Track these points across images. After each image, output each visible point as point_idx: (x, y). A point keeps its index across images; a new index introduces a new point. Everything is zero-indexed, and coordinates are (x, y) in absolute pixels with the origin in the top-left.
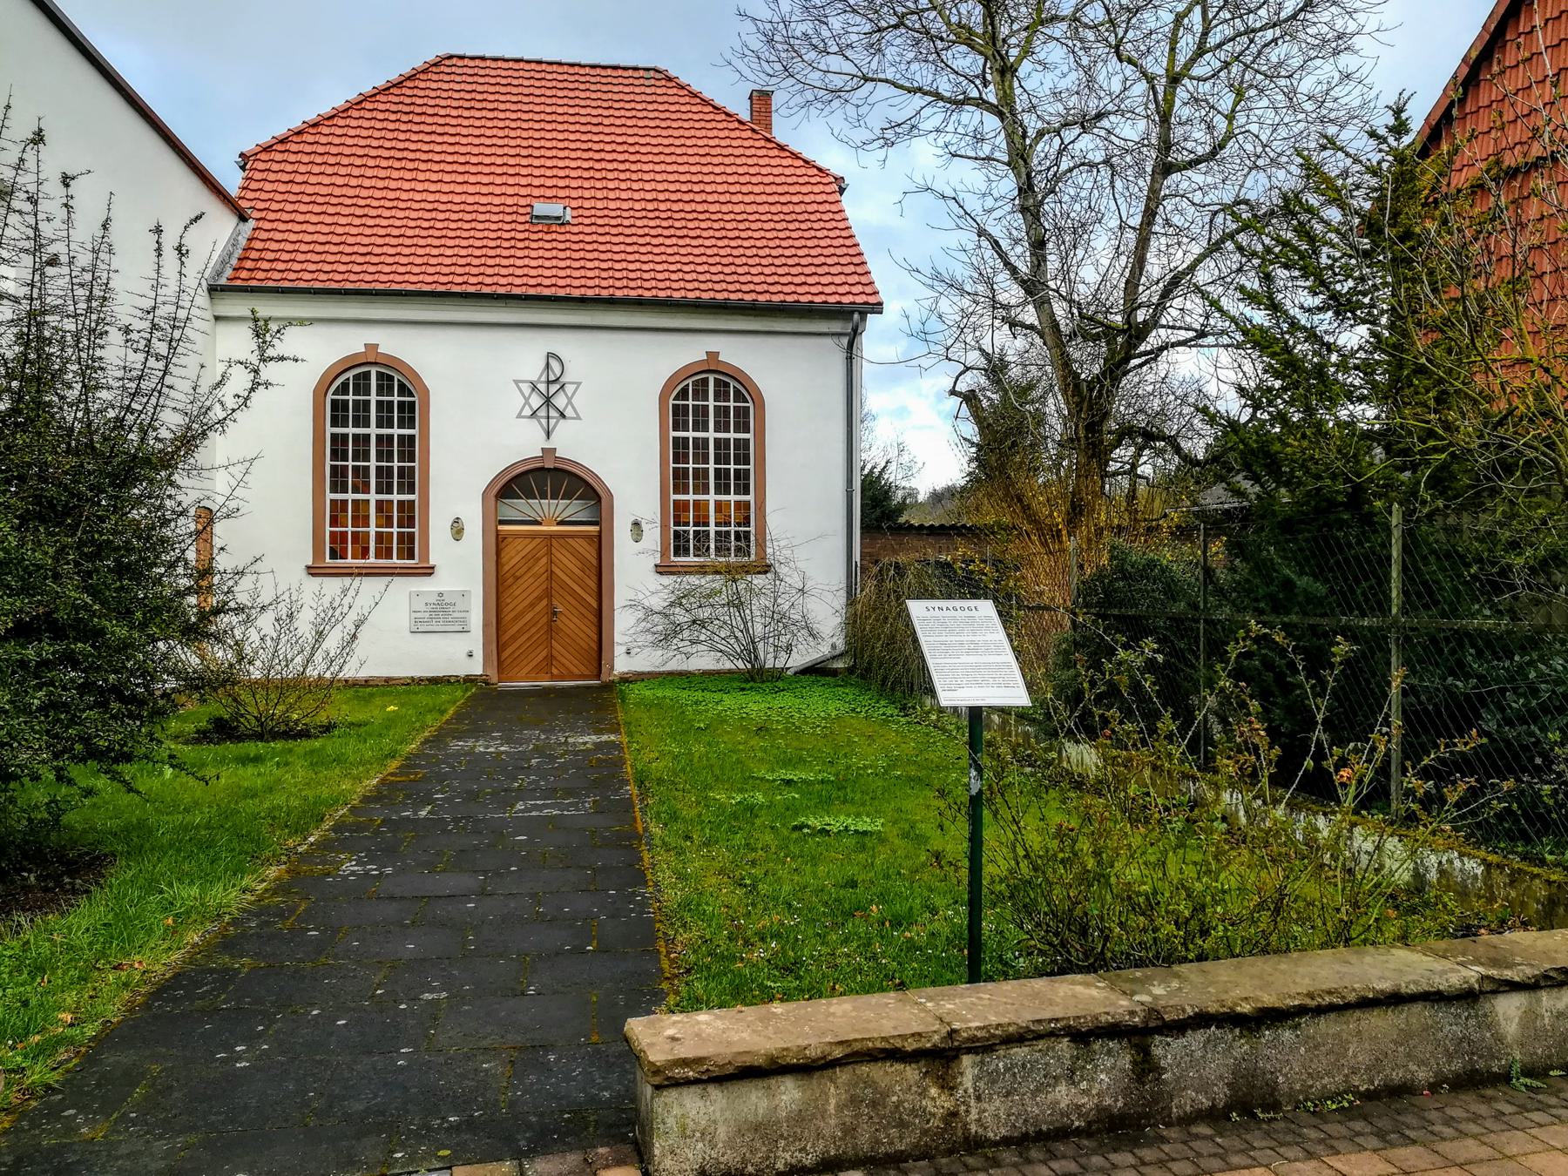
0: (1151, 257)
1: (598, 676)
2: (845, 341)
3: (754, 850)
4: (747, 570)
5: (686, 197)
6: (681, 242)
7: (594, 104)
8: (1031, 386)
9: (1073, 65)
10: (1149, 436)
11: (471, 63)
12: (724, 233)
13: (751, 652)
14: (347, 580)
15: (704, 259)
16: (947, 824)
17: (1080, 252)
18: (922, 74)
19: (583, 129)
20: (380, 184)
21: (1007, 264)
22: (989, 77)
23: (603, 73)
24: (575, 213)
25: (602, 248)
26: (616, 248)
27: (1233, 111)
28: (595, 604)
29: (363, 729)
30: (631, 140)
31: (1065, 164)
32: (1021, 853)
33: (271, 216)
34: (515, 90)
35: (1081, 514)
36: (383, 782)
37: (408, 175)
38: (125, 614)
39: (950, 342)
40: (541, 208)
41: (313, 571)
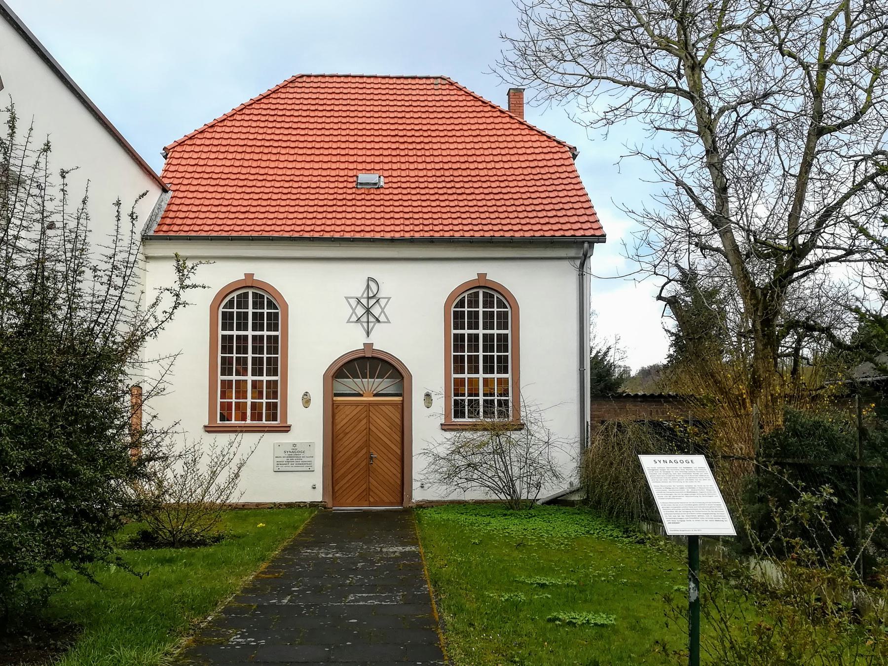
0: (808, 196)
1: (401, 503)
2: (578, 262)
3: (520, 636)
4: (506, 427)
5: (464, 166)
6: (460, 198)
7: (399, 103)
8: (716, 291)
9: (746, 60)
10: (810, 329)
11: (316, 80)
12: (490, 190)
13: (510, 485)
14: (233, 435)
15: (476, 209)
16: (670, 622)
17: (755, 196)
18: (634, 73)
19: (392, 121)
20: (255, 164)
21: (699, 205)
22: (682, 72)
23: (406, 82)
24: (387, 180)
25: (406, 204)
26: (415, 204)
27: (871, 86)
28: (399, 452)
29: (241, 541)
30: (425, 128)
31: (740, 132)
32: (727, 644)
33: (183, 188)
34: (345, 97)
35: (760, 387)
36: (257, 577)
37: (274, 158)
38: (91, 460)
39: (656, 263)
40: (363, 177)
41: (209, 429)
